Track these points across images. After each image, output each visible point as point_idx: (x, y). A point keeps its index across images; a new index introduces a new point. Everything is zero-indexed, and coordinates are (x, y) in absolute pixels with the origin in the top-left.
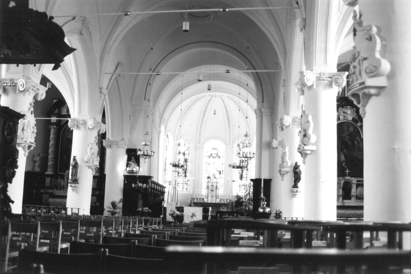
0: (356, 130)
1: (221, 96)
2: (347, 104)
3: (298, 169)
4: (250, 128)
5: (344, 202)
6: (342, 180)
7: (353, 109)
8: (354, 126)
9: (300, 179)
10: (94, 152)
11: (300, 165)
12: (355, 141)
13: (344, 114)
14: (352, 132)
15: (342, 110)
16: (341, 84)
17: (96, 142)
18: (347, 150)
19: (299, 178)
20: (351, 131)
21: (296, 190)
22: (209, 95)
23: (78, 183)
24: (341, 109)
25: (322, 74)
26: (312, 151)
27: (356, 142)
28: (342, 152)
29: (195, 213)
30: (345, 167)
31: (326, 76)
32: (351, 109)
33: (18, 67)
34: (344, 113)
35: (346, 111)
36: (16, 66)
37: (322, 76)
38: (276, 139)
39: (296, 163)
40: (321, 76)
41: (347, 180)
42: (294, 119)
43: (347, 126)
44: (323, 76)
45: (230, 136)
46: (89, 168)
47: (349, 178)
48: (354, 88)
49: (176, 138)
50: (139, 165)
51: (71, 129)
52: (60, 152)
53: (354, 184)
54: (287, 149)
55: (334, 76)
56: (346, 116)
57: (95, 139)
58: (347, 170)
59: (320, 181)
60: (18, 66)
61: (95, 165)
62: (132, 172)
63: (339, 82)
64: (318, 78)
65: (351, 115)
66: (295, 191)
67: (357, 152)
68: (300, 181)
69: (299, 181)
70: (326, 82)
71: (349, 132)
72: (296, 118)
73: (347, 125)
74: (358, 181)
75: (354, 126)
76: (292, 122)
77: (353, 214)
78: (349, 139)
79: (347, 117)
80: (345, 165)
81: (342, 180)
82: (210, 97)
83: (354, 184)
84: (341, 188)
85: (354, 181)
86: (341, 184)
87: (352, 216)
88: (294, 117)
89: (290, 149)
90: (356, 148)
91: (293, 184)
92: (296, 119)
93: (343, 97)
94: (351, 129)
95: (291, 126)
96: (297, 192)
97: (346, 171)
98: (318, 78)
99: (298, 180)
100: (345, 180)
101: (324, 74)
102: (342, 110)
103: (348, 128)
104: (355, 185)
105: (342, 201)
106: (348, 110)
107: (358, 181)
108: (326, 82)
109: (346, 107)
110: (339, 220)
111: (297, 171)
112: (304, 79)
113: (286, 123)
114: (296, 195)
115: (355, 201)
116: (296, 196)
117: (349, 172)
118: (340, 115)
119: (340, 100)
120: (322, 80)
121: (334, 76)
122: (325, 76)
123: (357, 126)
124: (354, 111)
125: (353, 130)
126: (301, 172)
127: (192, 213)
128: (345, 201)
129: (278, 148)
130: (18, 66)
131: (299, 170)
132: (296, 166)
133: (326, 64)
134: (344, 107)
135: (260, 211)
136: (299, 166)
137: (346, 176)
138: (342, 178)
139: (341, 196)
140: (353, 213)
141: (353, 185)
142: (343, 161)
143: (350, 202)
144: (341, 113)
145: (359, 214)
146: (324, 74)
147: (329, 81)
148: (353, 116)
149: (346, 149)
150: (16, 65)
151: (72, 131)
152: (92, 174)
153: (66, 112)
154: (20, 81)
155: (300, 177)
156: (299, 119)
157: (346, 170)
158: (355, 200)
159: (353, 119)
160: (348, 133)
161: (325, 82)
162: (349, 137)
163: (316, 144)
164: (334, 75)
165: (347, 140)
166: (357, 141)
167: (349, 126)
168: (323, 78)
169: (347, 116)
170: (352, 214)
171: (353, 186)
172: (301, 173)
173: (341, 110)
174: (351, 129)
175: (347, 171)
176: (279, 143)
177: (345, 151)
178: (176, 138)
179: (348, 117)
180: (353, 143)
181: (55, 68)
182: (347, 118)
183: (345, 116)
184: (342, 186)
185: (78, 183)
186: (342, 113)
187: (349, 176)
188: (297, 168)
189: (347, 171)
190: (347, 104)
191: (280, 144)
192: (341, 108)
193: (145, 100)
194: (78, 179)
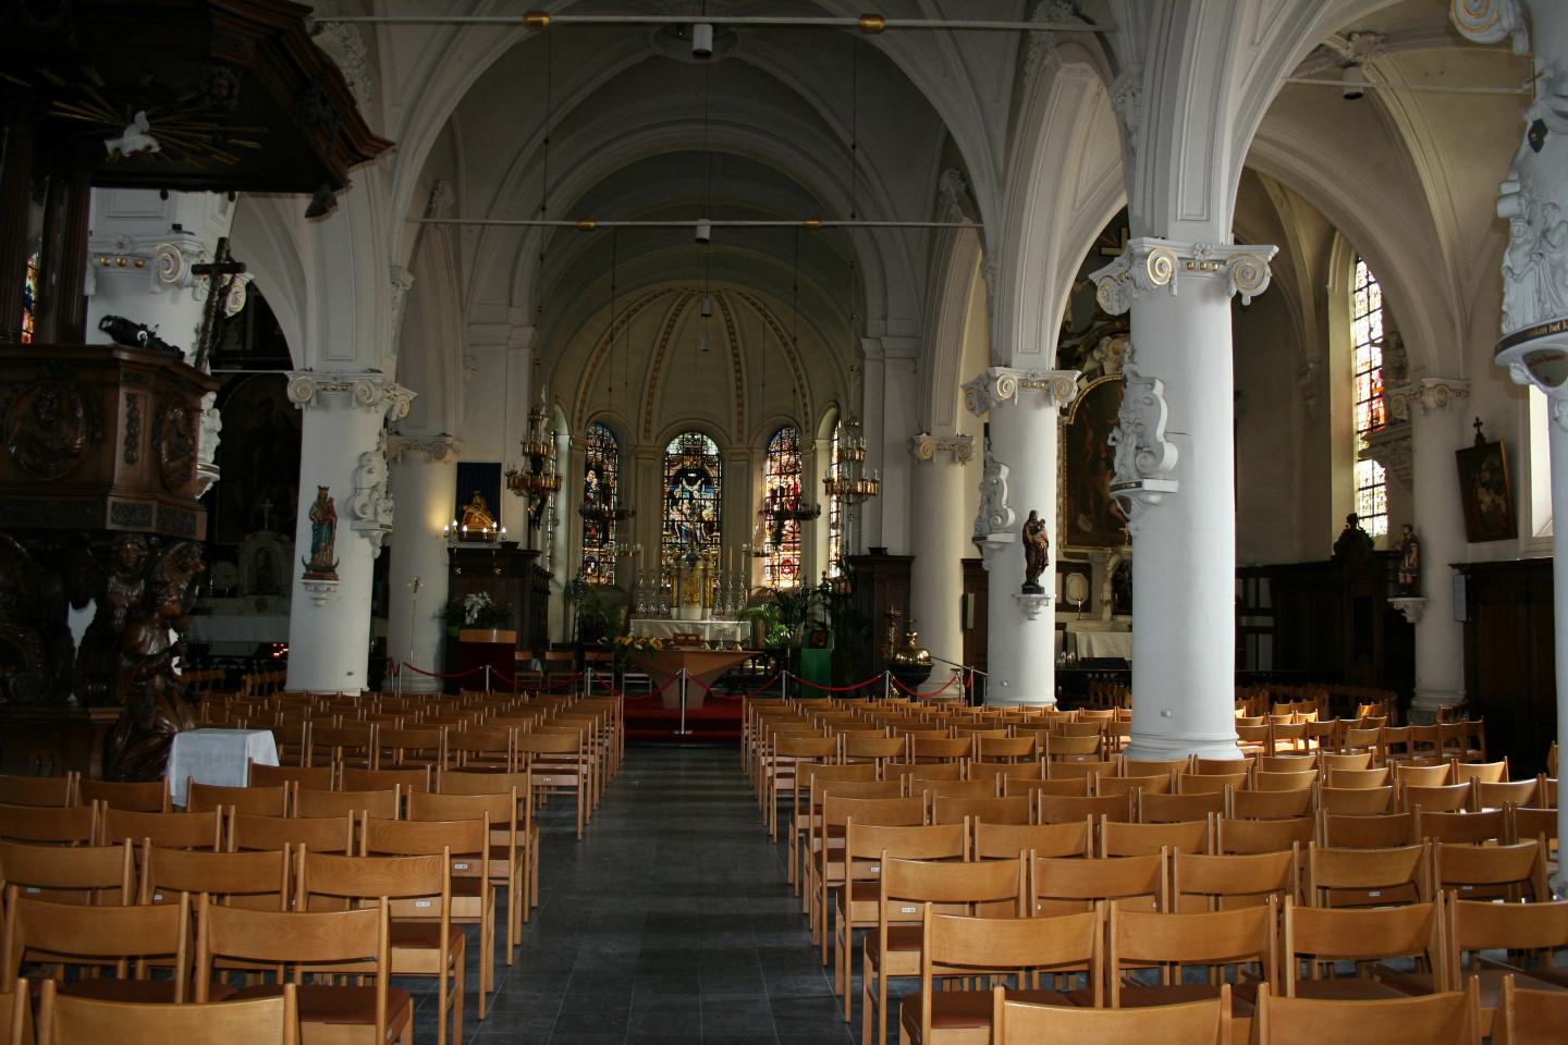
1: (719, 291)
4: (808, 400)
6: (1112, 555)
10: (378, 483)
11: (1043, 521)
17: (381, 451)
23: (336, 578)
24: (1110, 342)
33: (166, 202)
36: (159, 196)
38: (928, 434)
39: (1033, 514)
45: (741, 423)
46: (362, 536)
48: (1555, 333)
49: (576, 423)
50: (496, 517)
51: (297, 407)
54: (1004, 472)
57: (377, 439)
60: (164, 196)
61: (381, 526)
62: (475, 536)
84: (1109, 580)
102: (1111, 345)
120: (1197, 271)
122: (1206, 258)
129: (935, 460)
130: (164, 196)
139: (1107, 602)
150: (156, 193)
151: (300, 411)
152: (374, 553)
153: (237, 343)
154: (161, 251)
173: (1108, 345)
178: (576, 423)
181: (317, 211)
184: (1110, 575)
185: (336, 578)
192: (1108, 338)
194: (337, 564)
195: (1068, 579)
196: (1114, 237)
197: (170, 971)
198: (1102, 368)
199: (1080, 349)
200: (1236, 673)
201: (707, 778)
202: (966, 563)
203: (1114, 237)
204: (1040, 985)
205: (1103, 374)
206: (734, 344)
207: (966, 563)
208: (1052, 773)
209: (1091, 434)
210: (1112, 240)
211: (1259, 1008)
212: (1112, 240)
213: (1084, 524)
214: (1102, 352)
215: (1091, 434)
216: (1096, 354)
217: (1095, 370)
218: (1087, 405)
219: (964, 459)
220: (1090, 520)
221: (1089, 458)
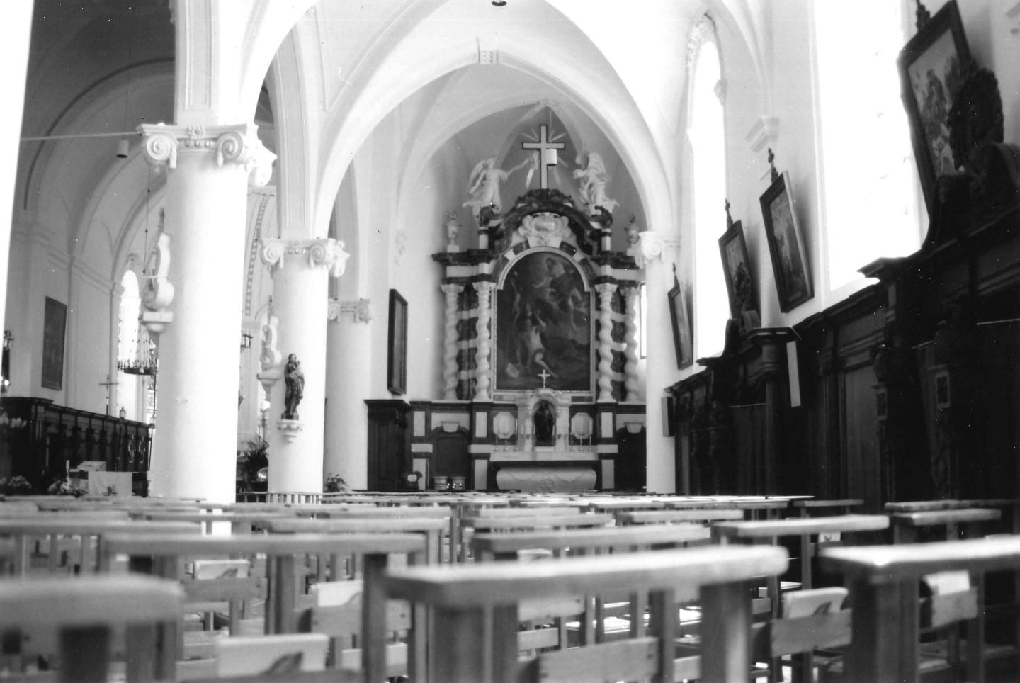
0: (572, 272)
2: (544, 208)
3: (294, 372)
5: (536, 452)
6: (532, 396)
7: (562, 220)
8: (566, 262)
9: (301, 397)
12: (567, 300)
13: (537, 232)
14: (561, 277)
15: (533, 224)
16: (238, 155)
18: (547, 323)
19: (296, 393)
20: (557, 276)
21: (287, 423)
22: (907, 208)
25: (191, 132)
26: (165, 324)
27: (570, 303)
28: (534, 328)
29: (114, 487)
30: (543, 364)
31: (203, 137)
32: (556, 219)
34: (539, 229)
35: (545, 224)
37: (192, 138)
40: (190, 136)
41: (545, 398)
42: (291, 247)
43: (550, 263)
44: (194, 136)
47: (549, 391)
52: (927, 341)
53: (562, 406)
55: (221, 135)
56: (543, 237)
58: (544, 371)
59: (179, 399)
63: (231, 149)
64: (183, 143)
65: (556, 235)
66: (285, 426)
67: (574, 326)
68: (302, 401)
69: (298, 403)
70: (204, 150)
71: (554, 276)
72: (295, 244)
73: (548, 259)
74: (574, 399)
75: (566, 262)
76: (284, 255)
77: (553, 483)
78: (552, 293)
79: (547, 239)
80: (544, 360)
81: (532, 396)
82: (262, 197)
83: (562, 406)
85: (562, 398)
86: (529, 408)
87: (550, 486)
88: (290, 242)
89: (281, 322)
90: (572, 317)
91: (283, 409)
92: (295, 247)
93: (537, 191)
94: (560, 270)
95: (282, 265)
96: (289, 428)
97: (544, 379)
98: (183, 143)
99: (294, 399)
100: (539, 396)
101: (196, 132)
103: (550, 268)
104: (568, 409)
105: (533, 449)
106: (548, 221)
107: (574, 399)
108: (204, 150)
109: (543, 215)
110: (326, 496)
111: (292, 376)
112: (146, 147)
113: (269, 257)
114: (290, 436)
115: (566, 448)
116: (291, 439)
117: (547, 378)
118: (529, 236)
119: (527, 198)
121: (221, 135)
123: (575, 261)
124: (563, 224)
125: (563, 272)
126: (302, 378)
127: (107, 485)
128: (539, 449)
129: (339, 320)
131: (296, 374)
132: (290, 365)
133: (210, 106)
134: (537, 216)
135: (259, 479)
136: (296, 364)
137: (541, 386)
138: (531, 391)
140: (554, 480)
141: (559, 408)
142: (539, 351)
143: (550, 453)
144: (530, 231)
145: (569, 480)
146: (196, 132)
147: (212, 149)
148: (563, 236)
149: (544, 320)
155: (299, 391)
156: (302, 246)
157: (542, 373)
158: (566, 445)
159: (564, 245)
160: (551, 279)
161: (198, 150)
162: (554, 290)
163: (174, 306)
164: (223, 132)
165: (548, 297)
166: (574, 298)
167: (554, 262)
168: (195, 141)
169: (546, 236)
170: (551, 480)
171: (559, 411)
172: (303, 382)
173: (530, 224)
174: (560, 270)
175: (544, 375)
176: (342, 308)
177: (543, 324)
179: (549, 241)
180: (564, 306)
182: (546, 243)
183: (541, 238)
186: (534, 231)
187: (548, 386)
188: (294, 369)
189: (544, 375)
190: (544, 208)
191: (343, 311)
193: (25, 207)
195: (495, 420)
196: (534, 132)
197: (326, 489)
198: (527, 242)
199: (503, 227)
200: (22, 144)
201: (992, 286)
202: (375, 407)
203: (534, 132)
204: (611, 247)
205: (528, 247)
206: (249, 298)
207: (375, 407)
208: (581, 389)
209: (518, 297)
210: (534, 136)
211: (607, 505)
212: (534, 136)
213: (512, 372)
214: (526, 229)
215: (518, 297)
216: (521, 230)
217: (521, 244)
218: (516, 274)
219: (365, 319)
220: (518, 368)
221: (517, 317)
